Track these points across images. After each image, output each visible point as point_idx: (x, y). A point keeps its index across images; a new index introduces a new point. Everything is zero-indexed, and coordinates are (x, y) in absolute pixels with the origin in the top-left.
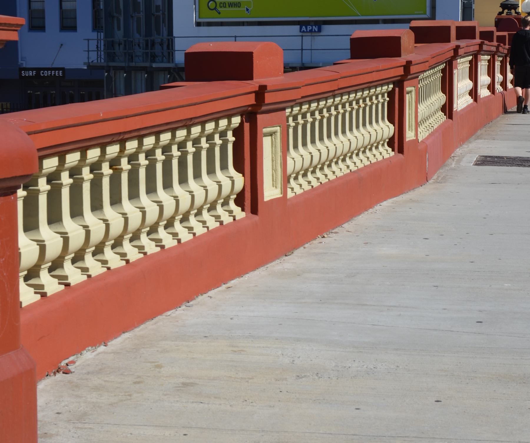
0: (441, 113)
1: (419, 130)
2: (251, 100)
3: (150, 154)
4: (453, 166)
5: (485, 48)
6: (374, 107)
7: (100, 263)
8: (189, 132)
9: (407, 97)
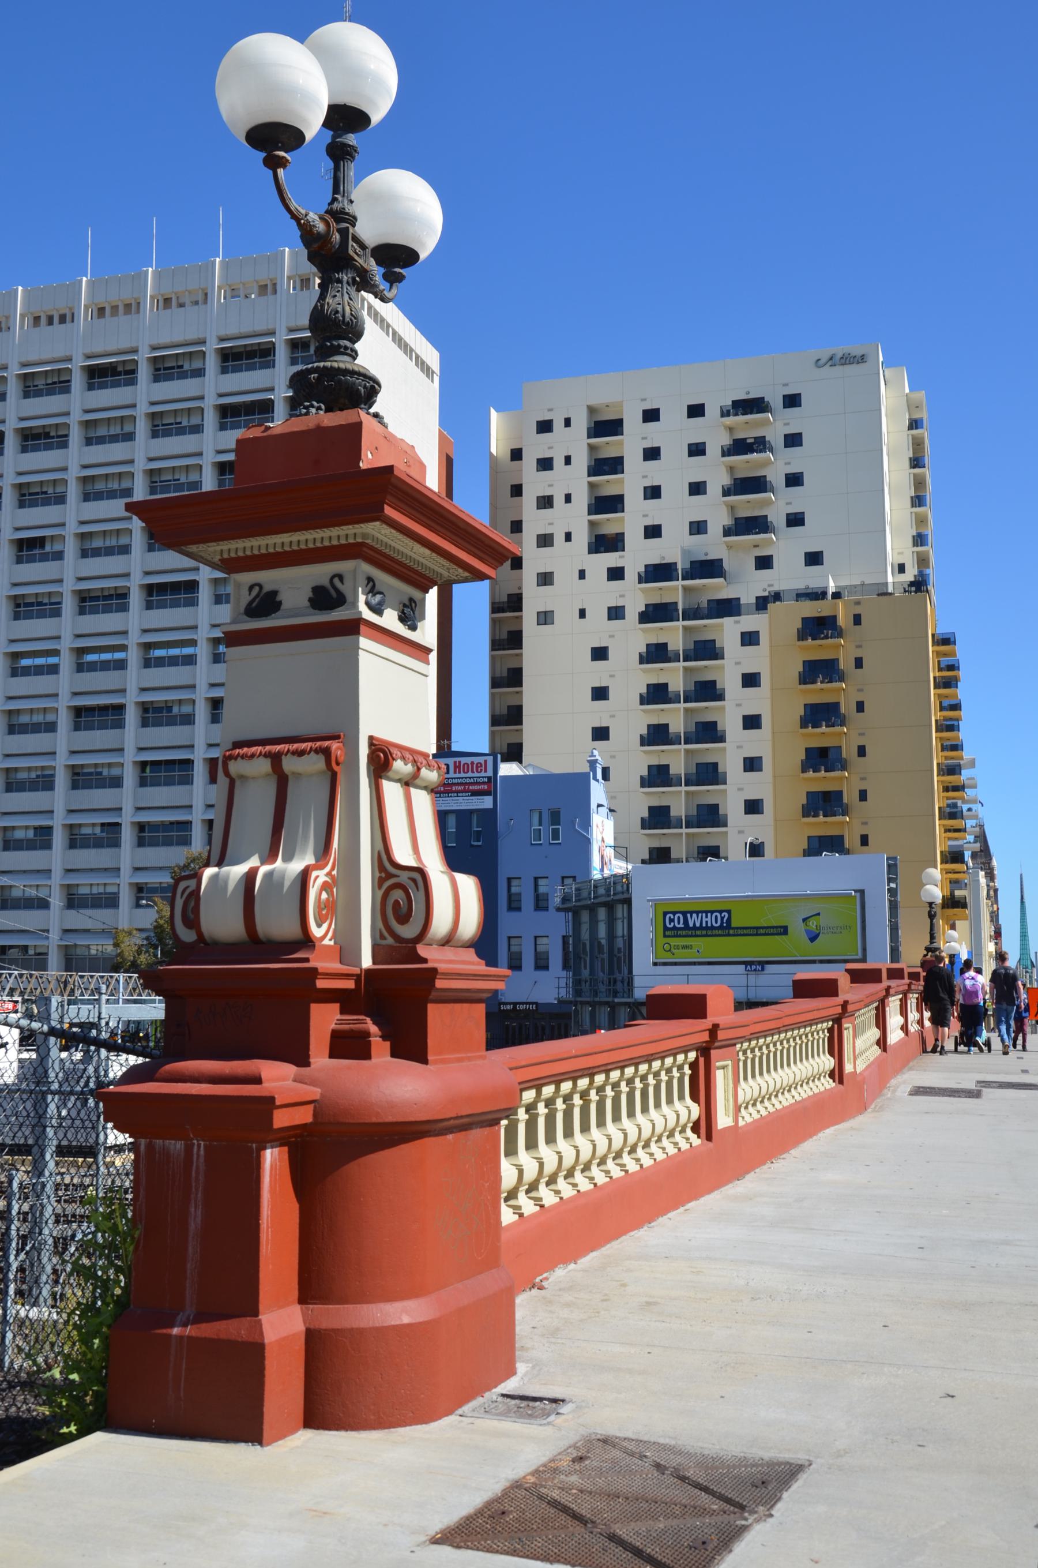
0: (876, 1047)
1: (857, 1063)
2: (706, 1037)
3: (615, 1086)
4: (889, 1096)
5: (913, 987)
6: (815, 1042)
7: (570, 1186)
8: (650, 1067)
9: (845, 1033)
